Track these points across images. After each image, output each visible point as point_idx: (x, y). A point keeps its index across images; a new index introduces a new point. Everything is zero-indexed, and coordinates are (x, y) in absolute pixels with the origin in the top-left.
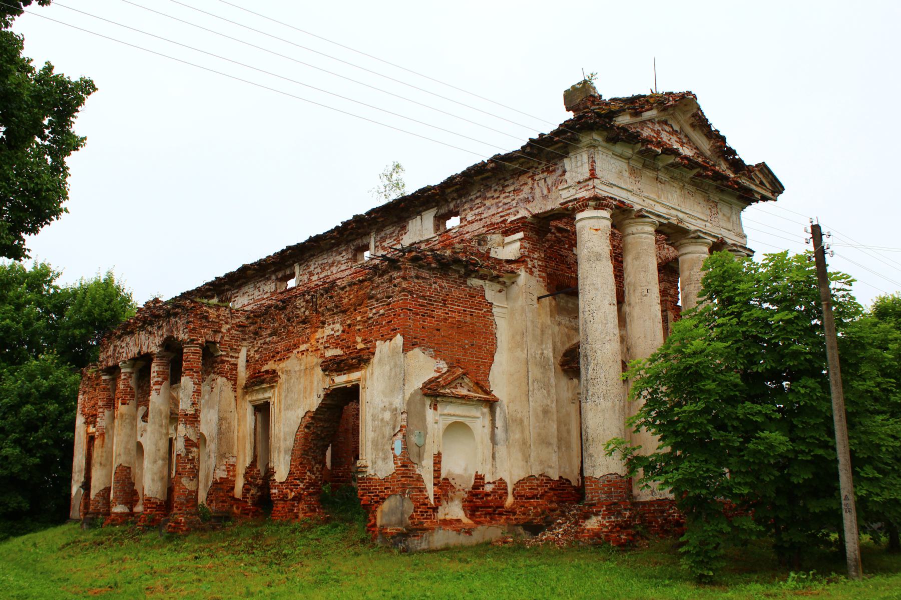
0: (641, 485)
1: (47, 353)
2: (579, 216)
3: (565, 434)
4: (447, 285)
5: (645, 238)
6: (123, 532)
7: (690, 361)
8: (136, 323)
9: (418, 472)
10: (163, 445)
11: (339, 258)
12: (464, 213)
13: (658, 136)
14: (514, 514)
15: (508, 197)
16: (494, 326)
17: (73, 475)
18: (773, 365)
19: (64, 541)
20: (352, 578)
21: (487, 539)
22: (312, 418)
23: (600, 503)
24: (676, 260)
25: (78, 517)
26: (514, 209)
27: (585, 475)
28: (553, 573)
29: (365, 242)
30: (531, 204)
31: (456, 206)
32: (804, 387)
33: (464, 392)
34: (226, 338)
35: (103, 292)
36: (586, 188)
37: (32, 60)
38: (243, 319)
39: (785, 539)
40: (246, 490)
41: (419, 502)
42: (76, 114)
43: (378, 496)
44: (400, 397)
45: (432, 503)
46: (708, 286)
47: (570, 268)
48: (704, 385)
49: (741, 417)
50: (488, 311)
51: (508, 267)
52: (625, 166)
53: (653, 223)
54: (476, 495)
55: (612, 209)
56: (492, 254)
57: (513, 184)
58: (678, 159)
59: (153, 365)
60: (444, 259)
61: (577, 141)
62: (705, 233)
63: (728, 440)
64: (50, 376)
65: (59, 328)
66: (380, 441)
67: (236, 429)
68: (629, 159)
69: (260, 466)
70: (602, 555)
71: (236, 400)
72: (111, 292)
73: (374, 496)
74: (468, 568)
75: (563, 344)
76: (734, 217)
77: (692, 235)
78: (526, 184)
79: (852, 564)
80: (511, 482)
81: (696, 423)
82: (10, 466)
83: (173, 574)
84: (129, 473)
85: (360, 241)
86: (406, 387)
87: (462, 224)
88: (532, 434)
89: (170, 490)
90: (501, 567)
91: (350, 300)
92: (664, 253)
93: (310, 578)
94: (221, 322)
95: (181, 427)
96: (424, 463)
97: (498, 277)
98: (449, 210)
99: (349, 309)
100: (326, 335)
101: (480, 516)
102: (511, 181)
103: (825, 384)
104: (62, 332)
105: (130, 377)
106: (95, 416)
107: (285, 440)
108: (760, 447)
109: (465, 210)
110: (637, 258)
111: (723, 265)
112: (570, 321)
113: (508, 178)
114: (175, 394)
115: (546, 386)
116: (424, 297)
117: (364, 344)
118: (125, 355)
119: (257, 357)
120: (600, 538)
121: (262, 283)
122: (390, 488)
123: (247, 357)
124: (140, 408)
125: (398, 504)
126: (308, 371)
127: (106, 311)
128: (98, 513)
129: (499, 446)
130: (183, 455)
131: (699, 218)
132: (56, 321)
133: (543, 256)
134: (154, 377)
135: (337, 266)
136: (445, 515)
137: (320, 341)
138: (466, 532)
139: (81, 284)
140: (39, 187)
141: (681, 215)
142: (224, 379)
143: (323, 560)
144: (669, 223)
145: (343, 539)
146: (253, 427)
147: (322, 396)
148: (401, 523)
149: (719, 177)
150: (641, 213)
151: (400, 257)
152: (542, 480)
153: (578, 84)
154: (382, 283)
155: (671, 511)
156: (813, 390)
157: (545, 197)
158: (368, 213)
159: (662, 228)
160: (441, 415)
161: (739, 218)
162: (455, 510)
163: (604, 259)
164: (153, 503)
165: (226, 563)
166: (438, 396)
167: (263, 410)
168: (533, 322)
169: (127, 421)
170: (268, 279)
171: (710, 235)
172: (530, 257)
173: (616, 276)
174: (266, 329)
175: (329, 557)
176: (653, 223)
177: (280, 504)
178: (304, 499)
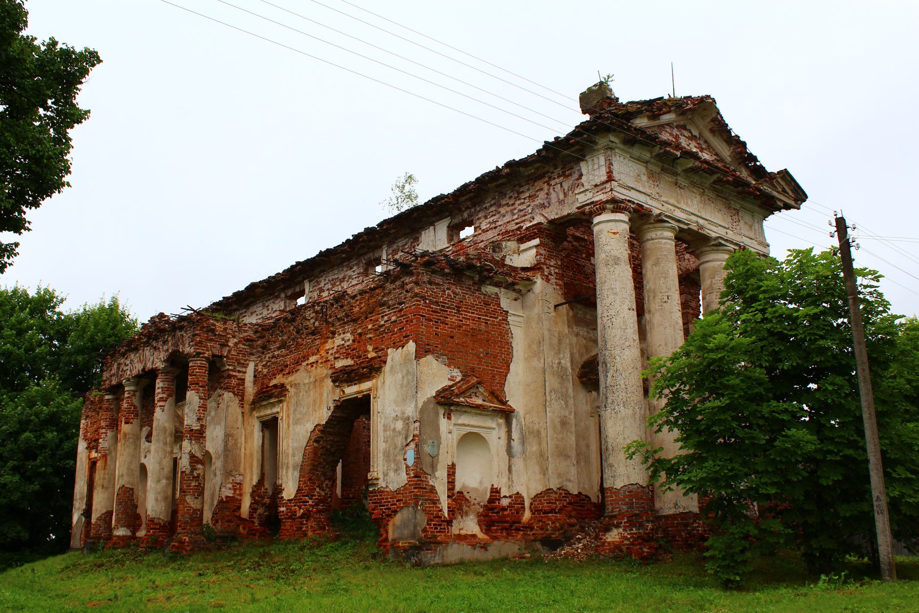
0: (664, 488)
1: (49, 379)
2: (596, 220)
3: (584, 449)
4: (460, 291)
5: (665, 243)
6: (124, 554)
7: (713, 356)
8: (140, 339)
9: (431, 483)
10: (167, 464)
11: (350, 273)
12: (478, 222)
13: (677, 140)
14: (532, 529)
15: (523, 203)
16: (510, 335)
17: (75, 502)
18: (799, 361)
19: (62, 567)
20: (362, 588)
21: (504, 554)
22: (322, 431)
23: (621, 515)
24: (697, 270)
25: (79, 546)
26: (530, 216)
27: (605, 486)
28: (572, 583)
29: (377, 255)
30: (547, 210)
31: (470, 215)
32: (832, 384)
33: (479, 401)
34: (233, 352)
35: (107, 317)
36: (603, 191)
37: (36, 39)
38: (251, 333)
39: (814, 546)
40: (253, 509)
41: (433, 514)
42: (79, 86)
43: (390, 509)
44: (413, 405)
45: (446, 515)
46: (730, 286)
47: (588, 278)
48: (728, 381)
49: (766, 416)
50: (503, 320)
51: (524, 275)
52: (643, 170)
53: (673, 228)
54: (492, 509)
55: (630, 212)
56: (508, 262)
57: (528, 190)
58: (697, 163)
59: (158, 381)
60: (457, 264)
61: (595, 143)
62: (726, 240)
63: (754, 438)
64: (51, 403)
65: (62, 355)
66: (392, 451)
67: (243, 446)
68: (647, 162)
69: (267, 485)
70: (624, 567)
71: (243, 416)
72: (115, 317)
73: (385, 509)
74: (483, 579)
75: (581, 355)
76: (756, 226)
77: (713, 243)
78: (541, 189)
79: (886, 568)
80: (528, 495)
81: (720, 420)
82: (9, 494)
83: (175, 587)
84: (132, 495)
85: (371, 254)
86: (419, 395)
87: (476, 233)
88: (549, 445)
89: (174, 513)
90: (517, 578)
91: (361, 308)
92: (684, 264)
93: (319, 589)
94: (228, 336)
95: (186, 444)
96: (437, 474)
97: (513, 284)
98: (462, 220)
99: (360, 317)
100: (336, 345)
101: (496, 531)
102: (527, 187)
103: (853, 383)
104: (64, 359)
105: (134, 395)
106: (97, 440)
107: (294, 455)
108: (786, 445)
109: (479, 219)
110: (657, 264)
111: (746, 264)
112: (588, 333)
113: (523, 184)
114: (180, 413)
115: (564, 396)
116: (437, 303)
117: (376, 352)
118: (129, 373)
119: (265, 371)
120: (621, 551)
121: (271, 301)
122: (402, 500)
123: (255, 372)
124: (144, 429)
125: (410, 516)
126: (318, 384)
127: (110, 336)
128: (99, 538)
129: (515, 459)
130: (188, 472)
131: (720, 225)
132: (58, 348)
133: (559, 263)
134: (159, 393)
135: (348, 281)
136: (460, 530)
137: (330, 352)
138: (482, 547)
139: (85, 310)
140: (41, 153)
141: (701, 222)
142: (231, 394)
143: (333, 575)
144: (689, 229)
145: (353, 555)
146: (260, 444)
147: (332, 408)
148: (413, 536)
149: (739, 183)
150: (660, 218)
151: (412, 261)
152: (561, 494)
153: (595, 86)
154: (394, 289)
155: (695, 525)
156: (841, 387)
157: (561, 202)
158: (380, 225)
159: (681, 235)
160: (455, 425)
161: (762, 227)
162: (470, 525)
163: (623, 263)
164: (156, 524)
165: (231, 578)
166: (452, 404)
167: (270, 426)
168: (550, 330)
169: (131, 440)
170: (277, 297)
171: (732, 242)
172: (546, 265)
173: (636, 288)
174: (275, 342)
175: (339, 572)
176: (673, 228)
177: (288, 523)
178: (313, 517)
